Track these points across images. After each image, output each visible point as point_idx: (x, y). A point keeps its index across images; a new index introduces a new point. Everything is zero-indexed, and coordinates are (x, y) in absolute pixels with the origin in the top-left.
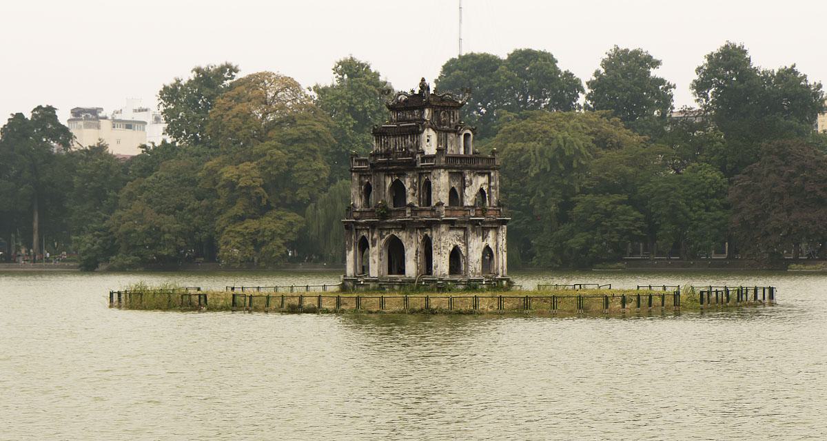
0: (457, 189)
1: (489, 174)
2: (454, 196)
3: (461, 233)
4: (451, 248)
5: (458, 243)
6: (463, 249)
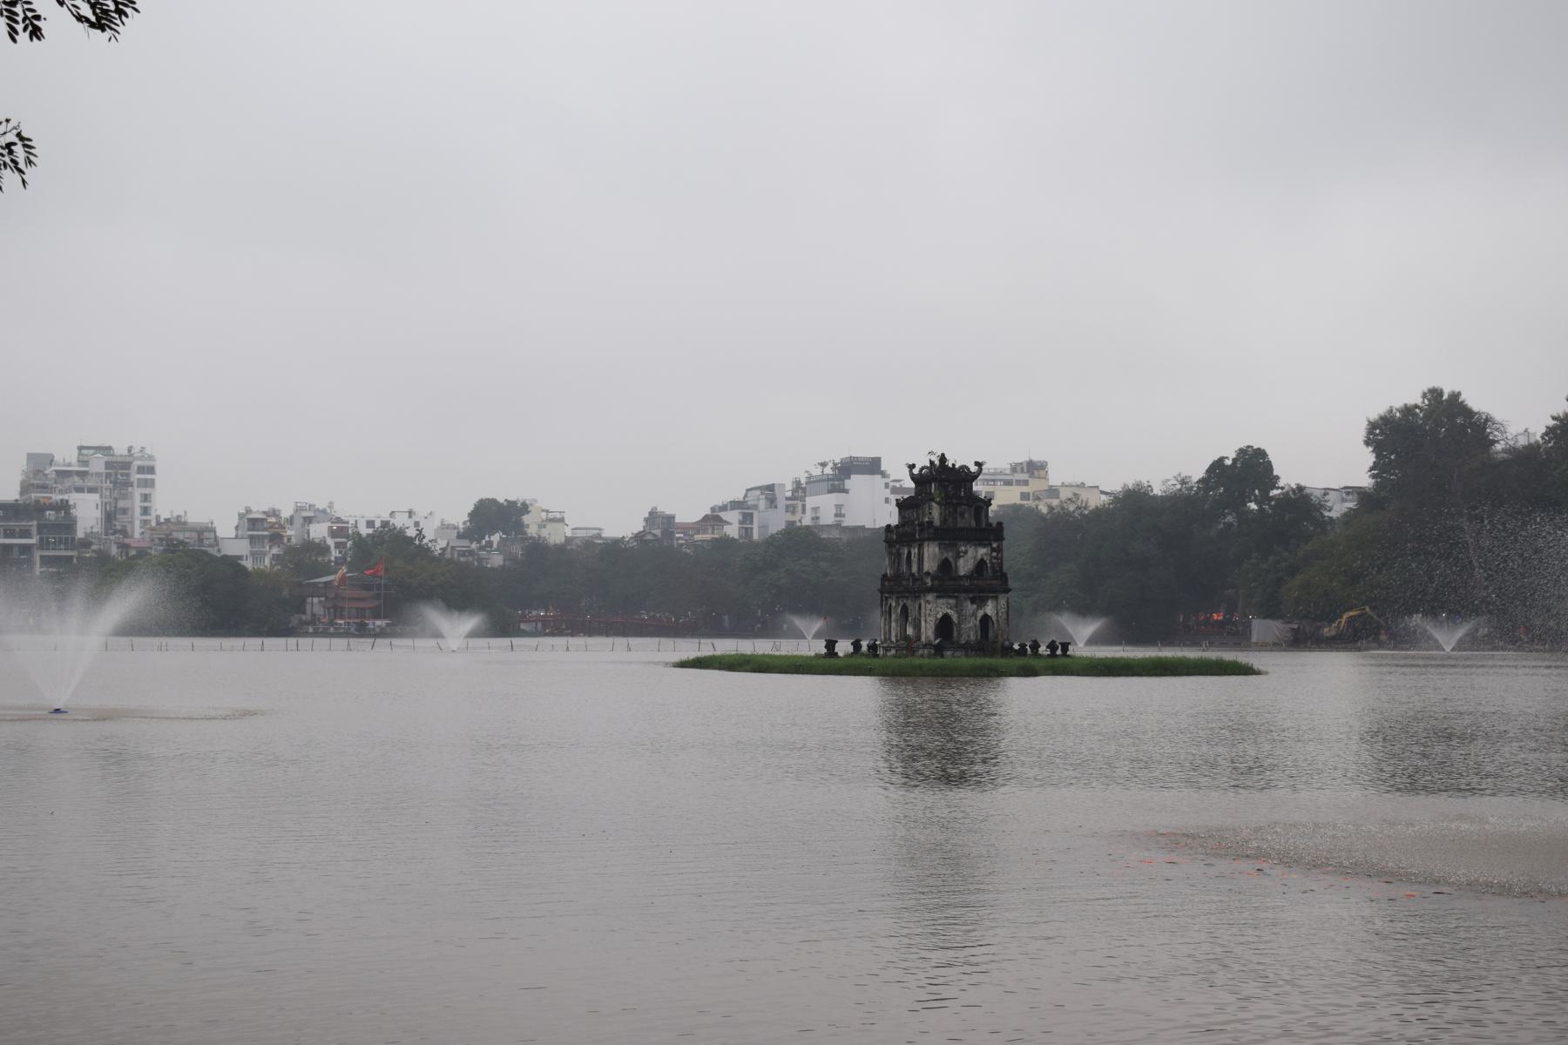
2: (945, 566)
3: (952, 601)
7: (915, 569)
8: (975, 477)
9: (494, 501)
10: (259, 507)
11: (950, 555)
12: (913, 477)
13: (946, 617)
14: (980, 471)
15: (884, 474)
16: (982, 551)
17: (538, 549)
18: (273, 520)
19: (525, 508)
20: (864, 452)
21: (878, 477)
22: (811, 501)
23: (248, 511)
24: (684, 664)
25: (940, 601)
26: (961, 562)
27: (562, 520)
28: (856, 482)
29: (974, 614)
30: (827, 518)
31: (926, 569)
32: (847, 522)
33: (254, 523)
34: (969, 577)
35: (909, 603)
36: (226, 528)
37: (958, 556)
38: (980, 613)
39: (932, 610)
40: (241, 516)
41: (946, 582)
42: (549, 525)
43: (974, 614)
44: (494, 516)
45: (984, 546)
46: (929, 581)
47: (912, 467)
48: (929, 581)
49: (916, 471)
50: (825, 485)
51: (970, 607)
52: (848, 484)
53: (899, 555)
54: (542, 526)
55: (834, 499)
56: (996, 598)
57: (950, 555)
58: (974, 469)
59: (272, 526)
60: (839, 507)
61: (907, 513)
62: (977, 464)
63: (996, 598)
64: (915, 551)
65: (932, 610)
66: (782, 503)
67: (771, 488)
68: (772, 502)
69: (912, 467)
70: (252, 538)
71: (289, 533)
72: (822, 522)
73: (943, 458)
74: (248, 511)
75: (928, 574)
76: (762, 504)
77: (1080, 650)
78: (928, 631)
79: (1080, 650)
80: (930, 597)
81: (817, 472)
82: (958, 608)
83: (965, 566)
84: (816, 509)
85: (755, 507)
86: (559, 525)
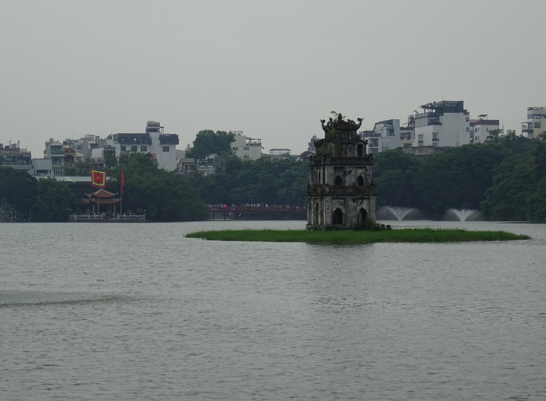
0: (341, 177)
1: (365, 168)
2: (339, 181)
3: (342, 201)
4: (334, 210)
5: (340, 207)
6: (343, 211)
7: (322, 183)
8: (358, 127)
9: (211, 132)
10: (60, 139)
11: (340, 174)
12: (324, 128)
13: (338, 210)
14: (360, 124)
15: (466, 112)
16: (360, 171)
17: (235, 165)
18: (68, 147)
19: (230, 137)
20: (452, 97)
21: (462, 114)
22: (418, 131)
23: (51, 140)
24: (188, 236)
25: (335, 201)
26: (347, 178)
27: (260, 144)
28: (447, 118)
29: (355, 208)
30: (428, 141)
31: (326, 182)
32: (441, 144)
33: (53, 147)
34: (353, 186)
35: (319, 202)
36: (38, 152)
37: (345, 174)
38: (359, 208)
39: (329, 206)
40: (47, 144)
41: (338, 189)
42: (251, 148)
43: (355, 208)
44: (212, 143)
45: (361, 168)
46: (327, 189)
47: (323, 121)
48: (327, 189)
49: (325, 124)
50: (426, 120)
51: (352, 204)
52: (442, 119)
53: (316, 174)
54: (246, 149)
55: (431, 129)
56: (369, 199)
57: (340, 174)
58: (357, 123)
59: (67, 150)
60: (435, 134)
61: (319, 149)
62: (360, 120)
63: (369, 199)
64: (322, 171)
65: (329, 206)
66: (397, 132)
67: (390, 122)
68: (391, 132)
69: (323, 121)
70: (52, 158)
71: (78, 154)
72: (425, 144)
73: (340, 116)
74: (51, 140)
75: (327, 185)
76: (385, 133)
77: (75, 218)
78: (328, 219)
79: (75, 218)
80: (328, 198)
81: (421, 111)
82: (344, 204)
83: (350, 180)
84: (421, 136)
85: (379, 135)
86: (258, 147)
